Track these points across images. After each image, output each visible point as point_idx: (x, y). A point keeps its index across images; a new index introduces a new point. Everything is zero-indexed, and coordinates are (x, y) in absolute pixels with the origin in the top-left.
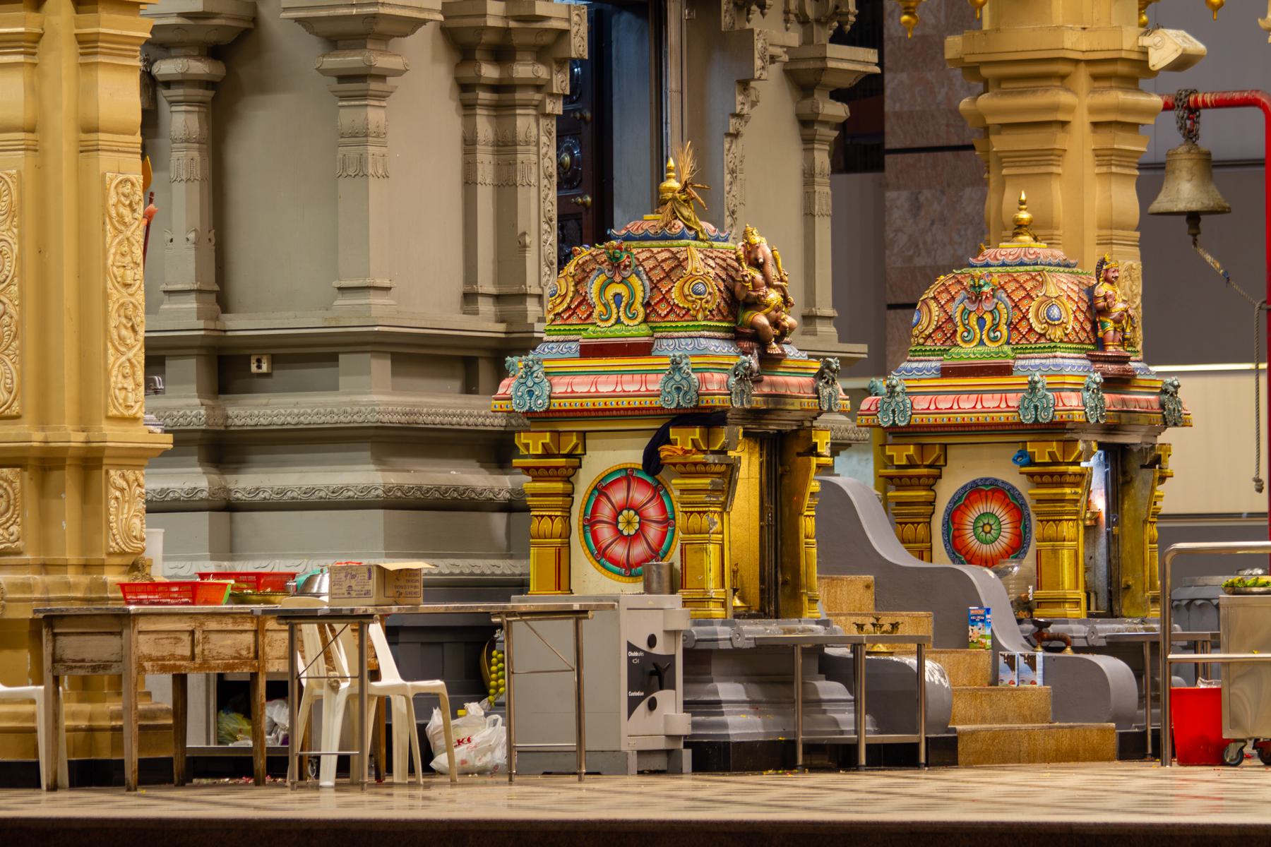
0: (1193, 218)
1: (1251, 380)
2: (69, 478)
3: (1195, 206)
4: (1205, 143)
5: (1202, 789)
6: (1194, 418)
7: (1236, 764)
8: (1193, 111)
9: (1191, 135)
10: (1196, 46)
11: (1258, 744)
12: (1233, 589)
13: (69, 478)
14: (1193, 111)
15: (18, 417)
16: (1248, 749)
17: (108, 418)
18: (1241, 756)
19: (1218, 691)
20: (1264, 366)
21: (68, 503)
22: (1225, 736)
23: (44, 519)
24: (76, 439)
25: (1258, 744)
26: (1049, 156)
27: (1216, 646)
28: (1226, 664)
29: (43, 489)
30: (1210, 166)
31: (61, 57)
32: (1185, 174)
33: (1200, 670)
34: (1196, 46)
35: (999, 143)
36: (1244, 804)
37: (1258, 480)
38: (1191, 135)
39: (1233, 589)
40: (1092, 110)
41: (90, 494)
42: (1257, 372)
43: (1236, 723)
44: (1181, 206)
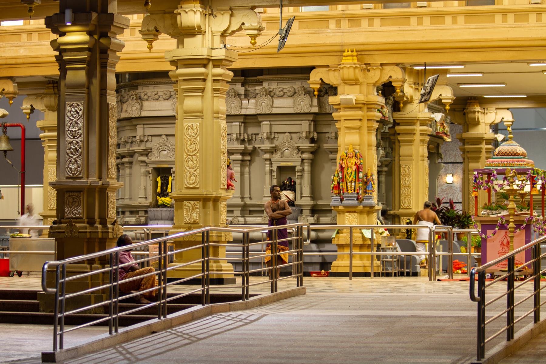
0: (5, 151)
1: (17, 189)
2: (211, 204)
3: (5, 149)
4: (8, 135)
5: (5, 282)
6: (4, 197)
7: (12, 276)
8: (6, 127)
9: (5, 133)
10: (6, 113)
11: (17, 272)
12: (12, 237)
13: (211, 204)
14: (6, 127)
15: (198, 188)
16: (15, 273)
17: (221, 188)
18: (14, 275)
19: (9, 260)
20: (20, 186)
21: (211, 211)
22: (10, 270)
23: (206, 215)
24: (214, 194)
25: (17, 272)
26: (411, 142)
27: (8, 250)
28: (11, 254)
29: (204, 207)
30: (9, 140)
31: (365, 131)
32: (3, 142)
33: (5, 255)
34: (6, 113)
35: (400, 138)
36: (14, 286)
37: (19, 212)
38: (5, 133)
39: (12, 237)
40: (421, 131)
41: (215, 208)
42: (19, 187)
43: (12, 267)
44: (2, 149)
